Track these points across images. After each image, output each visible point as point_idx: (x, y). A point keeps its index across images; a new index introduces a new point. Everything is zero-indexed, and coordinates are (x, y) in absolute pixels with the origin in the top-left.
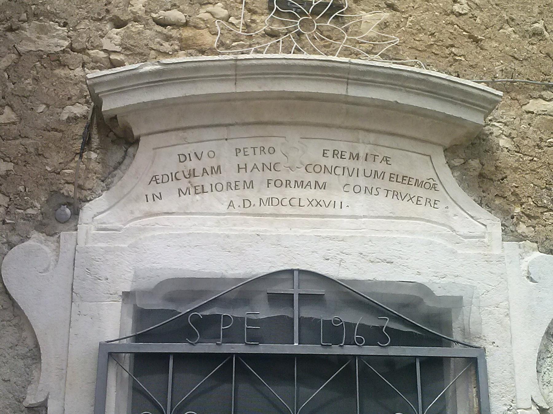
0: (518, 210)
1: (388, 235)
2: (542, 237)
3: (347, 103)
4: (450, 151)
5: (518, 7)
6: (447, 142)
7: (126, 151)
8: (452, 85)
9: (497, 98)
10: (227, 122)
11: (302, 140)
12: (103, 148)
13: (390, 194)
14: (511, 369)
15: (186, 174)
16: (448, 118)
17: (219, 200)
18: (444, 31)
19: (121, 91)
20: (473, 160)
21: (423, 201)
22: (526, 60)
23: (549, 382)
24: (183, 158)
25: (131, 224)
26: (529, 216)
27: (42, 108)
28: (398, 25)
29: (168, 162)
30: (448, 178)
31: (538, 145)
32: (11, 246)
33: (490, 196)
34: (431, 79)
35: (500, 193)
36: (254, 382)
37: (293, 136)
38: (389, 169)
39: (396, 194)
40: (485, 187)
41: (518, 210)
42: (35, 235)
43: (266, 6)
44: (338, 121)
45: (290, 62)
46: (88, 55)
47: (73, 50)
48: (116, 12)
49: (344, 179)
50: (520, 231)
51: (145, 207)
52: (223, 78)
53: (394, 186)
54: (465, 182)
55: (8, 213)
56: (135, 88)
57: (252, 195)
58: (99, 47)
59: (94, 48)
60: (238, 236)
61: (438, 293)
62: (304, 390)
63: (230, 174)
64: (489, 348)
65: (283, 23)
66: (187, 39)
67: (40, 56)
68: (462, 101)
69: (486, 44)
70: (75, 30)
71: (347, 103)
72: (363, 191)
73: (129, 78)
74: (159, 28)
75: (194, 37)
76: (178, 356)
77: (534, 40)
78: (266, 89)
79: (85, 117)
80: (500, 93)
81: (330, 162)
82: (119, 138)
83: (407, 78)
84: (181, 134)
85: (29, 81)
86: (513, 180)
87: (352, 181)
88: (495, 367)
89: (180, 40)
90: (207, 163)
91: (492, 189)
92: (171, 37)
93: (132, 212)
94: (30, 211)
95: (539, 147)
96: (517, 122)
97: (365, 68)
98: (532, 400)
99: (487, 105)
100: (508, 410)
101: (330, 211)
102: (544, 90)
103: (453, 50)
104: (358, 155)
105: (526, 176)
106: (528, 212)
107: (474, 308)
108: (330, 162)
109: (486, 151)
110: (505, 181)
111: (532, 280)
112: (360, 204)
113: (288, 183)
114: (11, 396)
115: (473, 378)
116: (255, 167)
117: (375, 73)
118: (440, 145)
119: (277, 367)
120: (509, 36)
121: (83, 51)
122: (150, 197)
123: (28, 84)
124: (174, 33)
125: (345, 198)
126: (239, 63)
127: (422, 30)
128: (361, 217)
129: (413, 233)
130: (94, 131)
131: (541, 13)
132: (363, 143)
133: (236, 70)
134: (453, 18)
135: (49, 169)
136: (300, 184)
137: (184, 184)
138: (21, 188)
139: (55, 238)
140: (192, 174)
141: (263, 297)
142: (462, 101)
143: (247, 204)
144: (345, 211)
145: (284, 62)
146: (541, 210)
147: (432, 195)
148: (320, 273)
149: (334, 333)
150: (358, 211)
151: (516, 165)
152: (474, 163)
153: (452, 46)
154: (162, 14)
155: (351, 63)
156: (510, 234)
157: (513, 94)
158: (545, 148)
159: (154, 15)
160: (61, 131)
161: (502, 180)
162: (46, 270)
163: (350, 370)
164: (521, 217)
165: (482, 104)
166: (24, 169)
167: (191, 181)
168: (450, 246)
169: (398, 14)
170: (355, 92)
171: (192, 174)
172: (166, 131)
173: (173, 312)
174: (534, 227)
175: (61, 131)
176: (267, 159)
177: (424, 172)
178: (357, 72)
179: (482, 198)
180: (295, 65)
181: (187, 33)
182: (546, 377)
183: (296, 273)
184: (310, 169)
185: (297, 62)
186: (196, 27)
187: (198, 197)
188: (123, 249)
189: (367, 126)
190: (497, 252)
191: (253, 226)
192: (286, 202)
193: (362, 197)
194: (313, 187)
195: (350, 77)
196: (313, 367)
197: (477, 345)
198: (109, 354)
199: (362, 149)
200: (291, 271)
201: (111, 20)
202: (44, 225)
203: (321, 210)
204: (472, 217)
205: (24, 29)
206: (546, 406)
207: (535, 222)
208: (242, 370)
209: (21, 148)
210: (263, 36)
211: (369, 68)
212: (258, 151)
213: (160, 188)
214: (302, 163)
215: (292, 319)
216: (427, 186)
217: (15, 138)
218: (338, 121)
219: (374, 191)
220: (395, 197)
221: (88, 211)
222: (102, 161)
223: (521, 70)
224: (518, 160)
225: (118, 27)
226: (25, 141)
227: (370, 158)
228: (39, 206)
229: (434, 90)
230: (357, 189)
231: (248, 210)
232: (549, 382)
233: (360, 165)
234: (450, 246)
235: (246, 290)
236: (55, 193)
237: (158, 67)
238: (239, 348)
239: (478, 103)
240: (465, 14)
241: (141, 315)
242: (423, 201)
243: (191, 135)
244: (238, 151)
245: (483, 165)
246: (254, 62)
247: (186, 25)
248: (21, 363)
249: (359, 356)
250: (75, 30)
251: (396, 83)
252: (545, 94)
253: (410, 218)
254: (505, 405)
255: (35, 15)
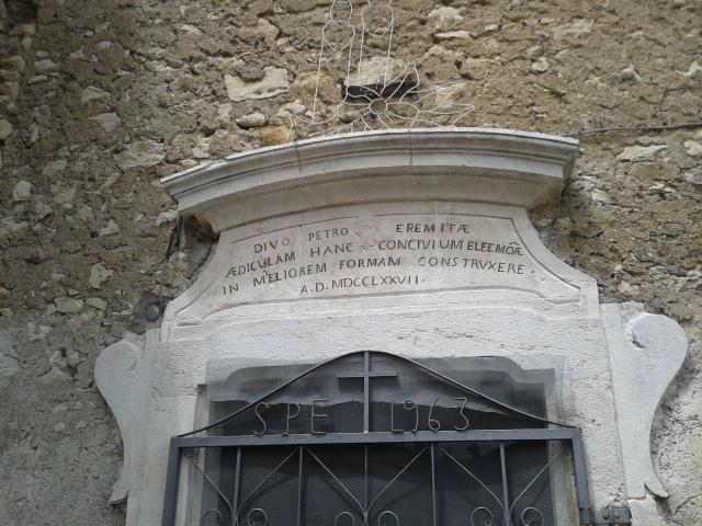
0: (619, 267)
1: (469, 307)
2: (649, 295)
3: (416, 174)
4: (535, 213)
5: (603, 55)
6: (530, 202)
7: (210, 249)
8: (521, 140)
9: (573, 147)
10: (300, 208)
11: (377, 219)
12: (190, 247)
13: (469, 263)
14: (619, 461)
15: (262, 263)
16: (523, 177)
17: (292, 286)
18: (523, 91)
19: (194, 190)
20: (561, 216)
21: (505, 267)
22: (617, 107)
23: (668, 465)
24: (259, 248)
25: (209, 318)
26: (631, 273)
27: (140, 217)
28: (474, 94)
29: (245, 254)
30: (532, 239)
31: (638, 195)
32: (106, 345)
33: (584, 255)
34: (497, 137)
35: (596, 251)
36: (324, 476)
37: (365, 215)
38: (466, 238)
39: (475, 263)
40: (577, 245)
41: (619, 267)
42: (129, 335)
43: (340, 96)
44: (409, 194)
45: (350, 141)
46: (181, 164)
47: (168, 162)
48: (205, 123)
49: (419, 253)
50: (622, 291)
51: (223, 299)
52: (287, 166)
53: (473, 254)
54: (553, 244)
55: (106, 316)
56: (206, 187)
57: (324, 278)
58: (191, 156)
59: (185, 157)
60: (309, 321)
61: (527, 366)
62: (376, 482)
63: (303, 259)
64: (588, 428)
65: (357, 108)
66: (266, 137)
67: (139, 171)
68: (536, 155)
69: (570, 98)
70: (170, 144)
71: (416, 174)
72: (439, 263)
73: (199, 177)
74: (242, 131)
75: (273, 134)
76: (246, 449)
77: (625, 85)
78: (329, 170)
79: (175, 220)
80: (576, 141)
81: (404, 236)
82: (205, 236)
83: (471, 140)
84: (258, 225)
85: (131, 194)
86: (610, 234)
87: (428, 254)
88: (596, 448)
89: (261, 139)
90: (282, 250)
91: (586, 247)
92: (252, 137)
93: (210, 306)
94: (124, 313)
95: (639, 196)
96: (611, 173)
97: (426, 136)
98: (646, 487)
99: (567, 158)
100: (616, 500)
101: (406, 287)
102: (640, 135)
103: (534, 108)
104: (433, 226)
105: (626, 229)
106: (630, 268)
107: (566, 381)
108: (404, 236)
109: (577, 208)
110: (601, 237)
111: (639, 345)
112: (436, 277)
113: (361, 263)
114: (98, 493)
115: (570, 463)
116: (328, 249)
117: (437, 139)
118: (522, 206)
119: (346, 457)
120: (596, 86)
121: (176, 162)
122: (228, 289)
123: (129, 197)
124: (255, 133)
125: (421, 272)
126: (299, 149)
127: (498, 94)
128: (438, 291)
129: (494, 303)
130: (183, 232)
131: (630, 57)
132: (439, 213)
133: (298, 156)
134: (532, 77)
135: (142, 272)
136: (374, 262)
137: (259, 274)
138: (118, 292)
139: (141, 337)
140: (267, 263)
141: (334, 384)
142: (536, 155)
143: (320, 287)
144: (421, 286)
145: (343, 141)
146: (645, 265)
147: (516, 260)
148: (390, 353)
149: (408, 417)
150: (434, 285)
151: (613, 218)
152: (564, 222)
153: (533, 105)
154: (245, 118)
155: (410, 133)
156: (607, 294)
157: (605, 144)
158: (646, 197)
159: (238, 120)
160: (155, 236)
161: (598, 236)
162: (133, 367)
163: (427, 454)
164: (623, 275)
165: (557, 156)
166: (122, 274)
167: (266, 270)
168: (536, 313)
169: (474, 82)
170: (420, 162)
171: (267, 263)
172: (244, 224)
173: (243, 403)
174: (639, 285)
175: (155, 236)
176: (339, 240)
177: (505, 236)
178: (419, 141)
179: (574, 258)
180: (354, 144)
181: (267, 131)
182: (664, 460)
183: (367, 355)
184: (384, 246)
185: (356, 140)
186: (275, 125)
187: (272, 285)
188: (198, 343)
189: (441, 196)
190: (593, 315)
191: (327, 309)
192: (359, 282)
193: (439, 269)
194: (387, 264)
195: (413, 147)
196: (384, 456)
197: (573, 424)
198: (182, 449)
199: (438, 220)
200: (361, 354)
201: (202, 131)
202: (136, 324)
203: (396, 287)
204: (563, 280)
205: (127, 150)
206: (664, 494)
207: (639, 279)
208: (309, 462)
209: (121, 255)
210: (339, 123)
211: (430, 136)
212: (330, 233)
213: (237, 280)
214: (375, 241)
215: (362, 405)
216: (510, 250)
217: (116, 247)
218: (409, 194)
219: (452, 262)
220: (474, 266)
221: (172, 307)
222: (188, 260)
223: (612, 118)
224: (615, 213)
225: (207, 135)
226: (123, 249)
227: (446, 228)
228: (132, 307)
229: (503, 148)
230: (434, 261)
231: (321, 294)
232: (668, 465)
233: (436, 236)
234: (536, 313)
235: (315, 376)
236: (148, 293)
237: (224, 163)
238: (307, 439)
239: (552, 155)
240: (545, 71)
241: (218, 407)
242: (505, 267)
243: (266, 225)
244: (311, 235)
245: (574, 222)
246: (314, 146)
247: (266, 124)
248: (109, 460)
249: (435, 443)
250: (170, 144)
251: (461, 146)
252: (641, 139)
253: (492, 287)
254: (611, 494)
255: (137, 136)
